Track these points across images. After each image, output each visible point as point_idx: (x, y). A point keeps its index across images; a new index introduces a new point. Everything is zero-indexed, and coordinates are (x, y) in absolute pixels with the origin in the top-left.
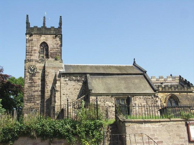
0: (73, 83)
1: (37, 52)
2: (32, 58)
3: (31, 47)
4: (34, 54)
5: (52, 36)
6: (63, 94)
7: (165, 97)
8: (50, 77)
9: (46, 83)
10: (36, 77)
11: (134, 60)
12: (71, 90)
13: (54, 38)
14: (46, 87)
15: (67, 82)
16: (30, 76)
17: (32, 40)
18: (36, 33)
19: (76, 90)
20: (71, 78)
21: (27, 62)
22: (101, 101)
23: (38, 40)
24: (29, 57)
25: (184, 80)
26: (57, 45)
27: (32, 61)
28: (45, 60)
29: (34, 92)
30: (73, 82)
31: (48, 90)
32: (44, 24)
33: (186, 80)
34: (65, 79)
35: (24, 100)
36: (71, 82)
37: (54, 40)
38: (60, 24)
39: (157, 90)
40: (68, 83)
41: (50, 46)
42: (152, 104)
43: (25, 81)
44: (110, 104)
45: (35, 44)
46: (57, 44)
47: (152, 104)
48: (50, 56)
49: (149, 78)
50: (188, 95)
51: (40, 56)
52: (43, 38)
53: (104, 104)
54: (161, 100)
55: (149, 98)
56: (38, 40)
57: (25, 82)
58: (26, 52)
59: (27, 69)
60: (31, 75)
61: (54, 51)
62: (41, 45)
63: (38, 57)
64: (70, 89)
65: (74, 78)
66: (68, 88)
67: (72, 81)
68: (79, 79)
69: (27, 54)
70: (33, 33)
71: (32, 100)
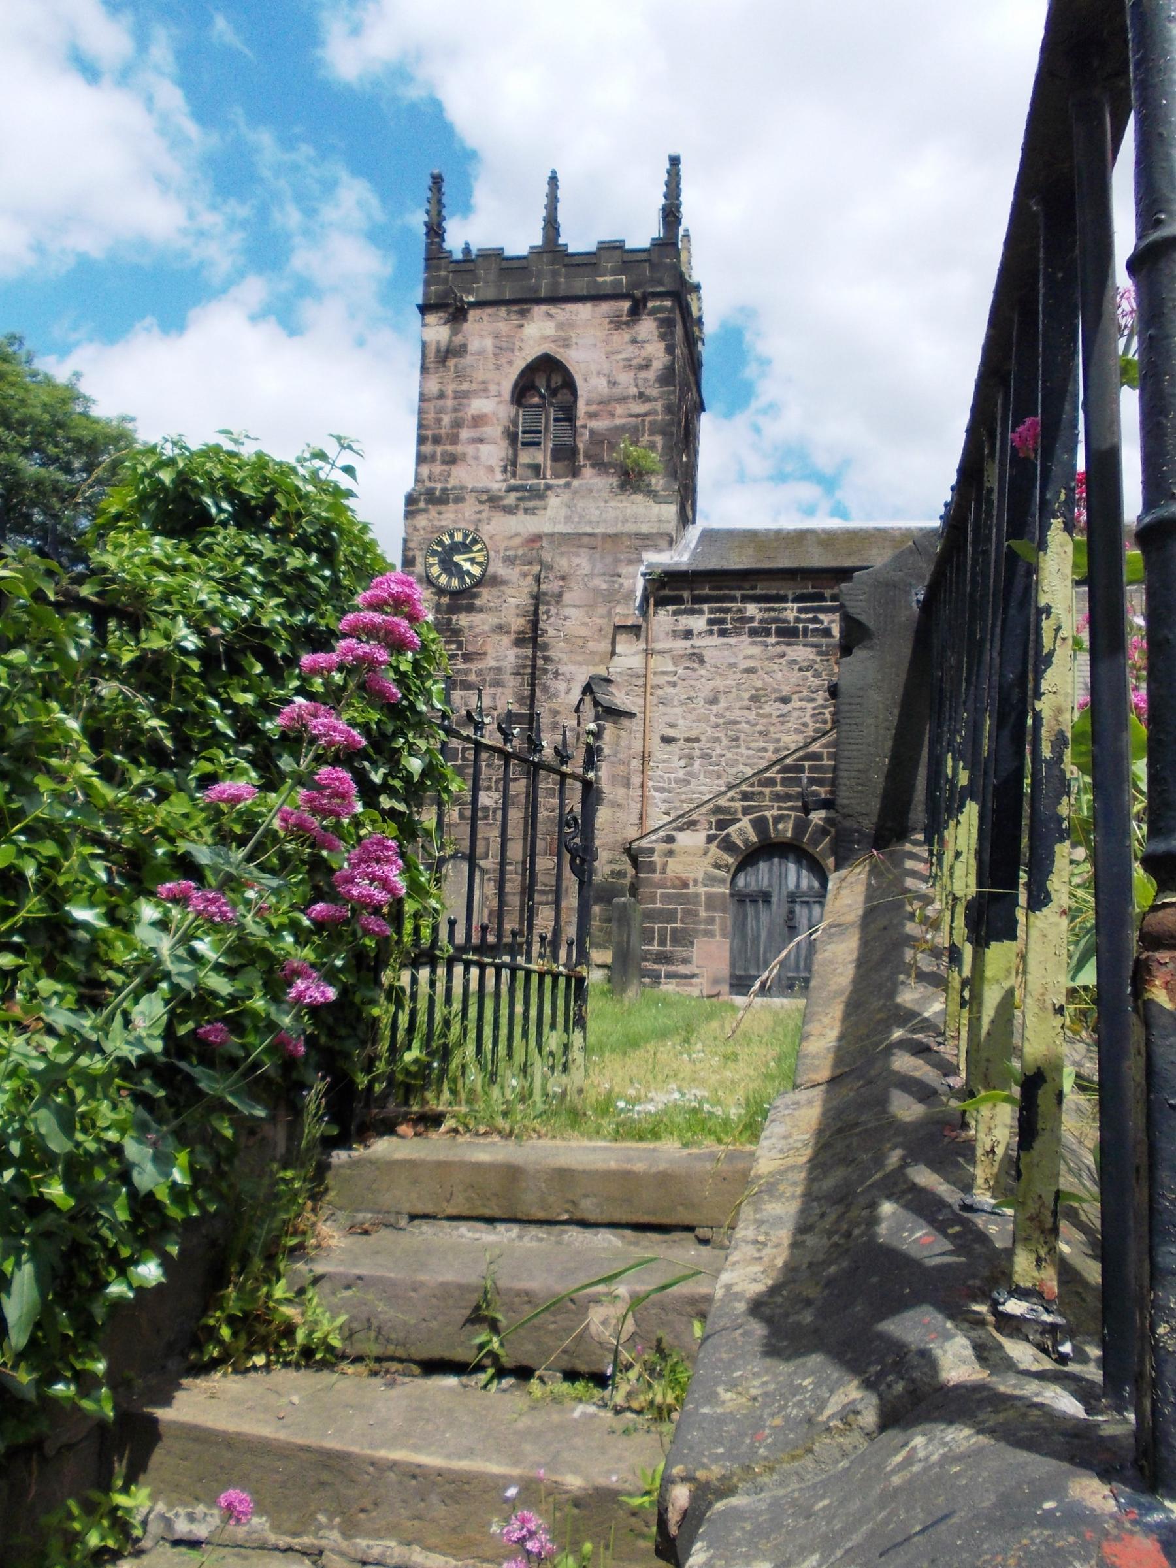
0: (744, 648)
1: (495, 431)
2: (461, 476)
3: (450, 403)
4: (470, 450)
5: (605, 307)
6: (667, 740)
8: (568, 611)
9: (547, 659)
10: (477, 618)
12: (723, 704)
13: (617, 324)
14: (545, 689)
15: (697, 642)
16: (438, 608)
18: (490, 294)
19: (767, 709)
20: (728, 610)
21: (422, 505)
23: (504, 347)
24: (438, 468)
26: (643, 374)
28: (548, 487)
30: (745, 639)
31: (555, 713)
32: (551, 225)
34: (688, 622)
36: (732, 640)
38: (671, 215)
40: (705, 653)
41: (590, 385)
45: (480, 375)
48: (587, 457)
51: (514, 463)
52: (538, 333)
56: (504, 347)
58: (421, 440)
59: (419, 560)
61: (618, 422)
62: (522, 390)
63: (498, 470)
64: (714, 701)
65: (752, 609)
66: (706, 693)
67: (737, 632)
70: (472, 299)
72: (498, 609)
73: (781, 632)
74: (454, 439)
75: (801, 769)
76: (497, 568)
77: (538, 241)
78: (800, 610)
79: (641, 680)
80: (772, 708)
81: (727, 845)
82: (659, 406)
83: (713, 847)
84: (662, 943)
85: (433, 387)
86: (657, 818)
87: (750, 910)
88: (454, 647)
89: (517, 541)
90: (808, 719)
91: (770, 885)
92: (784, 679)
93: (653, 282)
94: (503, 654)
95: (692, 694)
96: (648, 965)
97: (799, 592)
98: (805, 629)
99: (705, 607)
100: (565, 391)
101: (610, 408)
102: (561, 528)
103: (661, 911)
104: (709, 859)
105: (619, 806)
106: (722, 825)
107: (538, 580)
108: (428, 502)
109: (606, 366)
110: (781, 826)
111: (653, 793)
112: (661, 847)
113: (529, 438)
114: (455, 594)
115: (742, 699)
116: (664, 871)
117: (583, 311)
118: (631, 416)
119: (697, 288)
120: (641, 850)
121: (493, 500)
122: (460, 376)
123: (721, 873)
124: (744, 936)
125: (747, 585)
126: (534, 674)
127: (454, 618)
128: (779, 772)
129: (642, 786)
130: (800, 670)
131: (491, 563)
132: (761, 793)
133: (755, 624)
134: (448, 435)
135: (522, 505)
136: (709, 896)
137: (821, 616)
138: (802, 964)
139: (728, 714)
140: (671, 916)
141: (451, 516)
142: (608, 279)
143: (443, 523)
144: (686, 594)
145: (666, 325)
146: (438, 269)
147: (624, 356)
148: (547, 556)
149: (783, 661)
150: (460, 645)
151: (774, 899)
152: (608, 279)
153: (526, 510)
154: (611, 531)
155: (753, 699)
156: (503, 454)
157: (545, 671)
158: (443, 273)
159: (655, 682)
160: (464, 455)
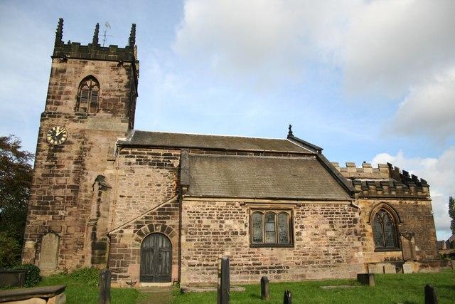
0: (148, 170)
1: (73, 96)
2: (60, 109)
4: (64, 101)
7: (368, 210)
8: (92, 154)
9: (84, 169)
10: (62, 154)
11: (290, 128)
12: (140, 186)
13: (114, 68)
20: (142, 157)
21: (47, 117)
22: (211, 218)
23: (78, 72)
24: (53, 106)
29: (56, 188)
32: (96, 38)
38: (132, 39)
41: (104, 85)
42: (345, 227)
44: (237, 227)
46: (120, 82)
47: (345, 227)
52: (89, 68)
53: (221, 226)
55: (337, 213)
56: (78, 72)
58: (48, 97)
61: (112, 97)
66: (135, 182)
68: (162, 160)
71: (48, 208)
74: (59, 98)
81: (140, 234)
82: (125, 94)
84: (118, 266)
85: (54, 81)
86: (118, 223)
90: (166, 192)
92: (160, 179)
93: (126, 58)
94: (71, 166)
96: (113, 273)
103: (118, 255)
104: (134, 238)
106: (139, 227)
107: (83, 143)
112: (118, 234)
116: (119, 242)
117: (104, 63)
119: (138, 62)
120: (112, 235)
122: (63, 79)
123: (137, 243)
124: (144, 263)
136: (134, 250)
140: (121, 257)
144: (130, 151)
145: (128, 72)
157: (83, 173)
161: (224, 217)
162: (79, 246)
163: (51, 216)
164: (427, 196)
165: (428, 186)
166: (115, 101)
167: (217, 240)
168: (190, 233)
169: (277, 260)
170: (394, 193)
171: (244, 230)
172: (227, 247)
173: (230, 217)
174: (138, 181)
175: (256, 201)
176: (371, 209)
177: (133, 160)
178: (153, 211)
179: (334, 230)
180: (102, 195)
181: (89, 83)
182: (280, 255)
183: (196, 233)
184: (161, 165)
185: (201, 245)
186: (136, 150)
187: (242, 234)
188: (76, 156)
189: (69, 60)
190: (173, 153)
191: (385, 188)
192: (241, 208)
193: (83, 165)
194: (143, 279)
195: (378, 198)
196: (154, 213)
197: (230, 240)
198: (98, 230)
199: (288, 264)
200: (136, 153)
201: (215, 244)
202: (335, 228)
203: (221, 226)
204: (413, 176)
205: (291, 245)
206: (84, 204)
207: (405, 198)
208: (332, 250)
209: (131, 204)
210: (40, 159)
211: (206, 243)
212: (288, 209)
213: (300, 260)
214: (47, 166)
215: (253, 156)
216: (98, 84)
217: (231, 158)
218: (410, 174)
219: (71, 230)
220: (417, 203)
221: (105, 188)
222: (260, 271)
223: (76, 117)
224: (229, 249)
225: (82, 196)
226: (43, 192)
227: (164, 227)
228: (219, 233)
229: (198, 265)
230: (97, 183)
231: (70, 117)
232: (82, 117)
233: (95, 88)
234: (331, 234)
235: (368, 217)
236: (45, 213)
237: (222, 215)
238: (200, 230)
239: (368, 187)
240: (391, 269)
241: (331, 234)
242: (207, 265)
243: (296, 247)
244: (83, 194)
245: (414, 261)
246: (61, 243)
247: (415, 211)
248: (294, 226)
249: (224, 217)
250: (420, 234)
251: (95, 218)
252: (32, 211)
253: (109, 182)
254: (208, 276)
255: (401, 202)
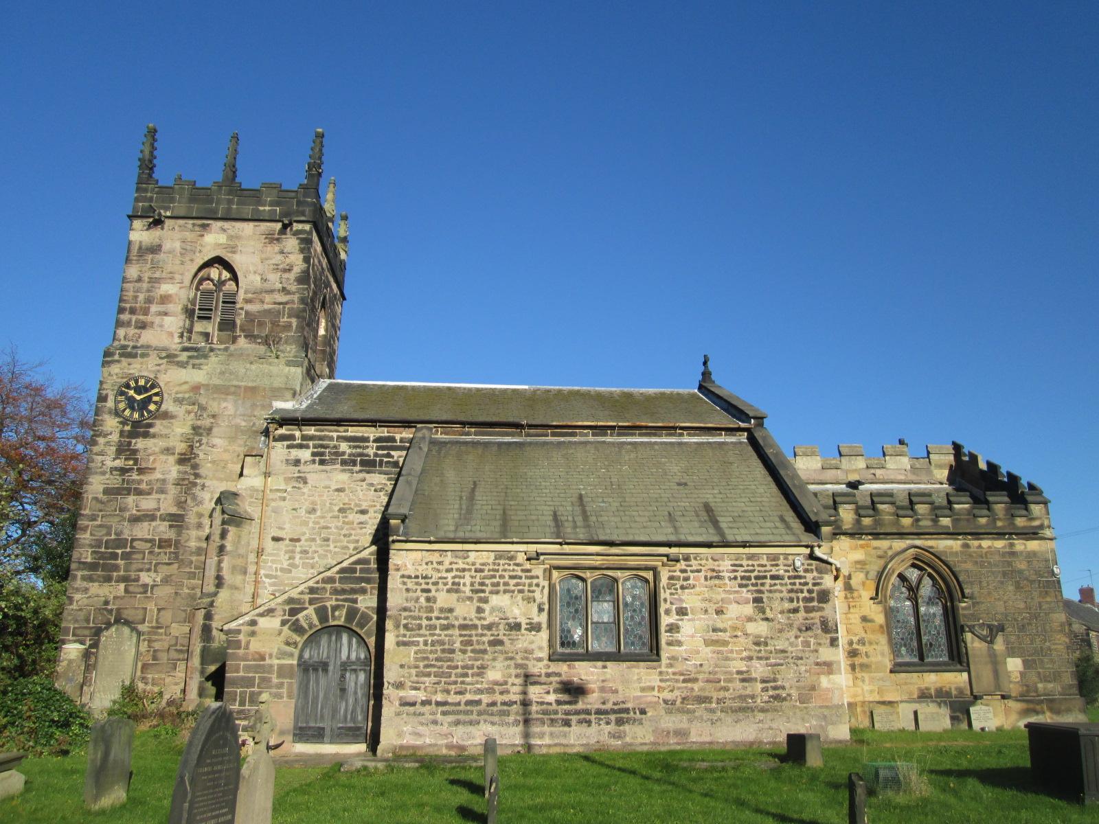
0: (339, 476)
1: (176, 308)
2: (147, 337)
3: (145, 286)
4: (157, 320)
5: (265, 226)
6: (276, 539)
7: (874, 568)
8: (216, 441)
9: (197, 476)
11: (705, 363)
12: (319, 513)
13: (271, 239)
16: (122, 433)
17: (160, 246)
21: (116, 357)
22: (457, 591)
23: (187, 251)
24: (132, 331)
25: (983, 466)
26: (286, 275)
27: (143, 356)
29: (135, 520)
31: (200, 515)
33: (993, 467)
35: (73, 566)
36: (328, 468)
37: (269, 248)
39: (827, 524)
40: (308, 476)
41: (250, 280)
42: (796, 611)
43: (93, 461)
44: (518, 610)
45: (169, 268)
46: (285, 271)
47: (796, 611)
48: (242, 330)
49: (779, 454)
50: (1013, 554)
51: (190, 331)
52: (215, 239)
53: (480, 610)
54: (848, 588)
55: (773, 577)
57: (91, 465)
58: (121, 310)
59: (111, 399)
60: (128, 428)
61: (266, 307)
63: (176, 335)
64: (313, 511)
66: (306, 505)
67: (333, 462)
68: (371, 452)
69: (125, 317)
70: (168, 214)
71: (116, 568)
72: (167, 436)
73: (363, 463)
74: (146, 312)
75: (354, 571)
76: (168, 406)
77: (219, 177)
78: (378, 448)
79: (262, 497)
80: (353, 517)
81: (297, 628)
82: (296, 298)
83: (286, 628)
84: (242, 703)
87: (312, 676)
88: (131, 462)
89: (185, 387)
91: (328, 657)
94: (169, 469)
95: (297, 506)
97: (378, 435)
98: (381, 462)
99: (311, 443)
100: (231, 282)
101: (261, 296)
102: (216, 381)
103: (243, 678)
104: (282, 638)
105: (236, 588)
106: (293, 612)
108: (121, 355)
109: (260, 268)
110: (337, 613)
111: (264, 579)
112: (245, 629)
113: (203, 313)
114: (136, 424)
115: (333, 511)
116: (247, 647)
117: (248, 228)
118: (275, 303)
121: (170, 357)
122: (155, 267)
125: (342, 429)
126: (188, 485)
127: (134, 441)
128: (338, 572)
129: (255, 574)
130: (375, 491)
131: (165, 402)
132: (324, 588)
133: (346, 457)
134: (141, 308)
135: (193, 361)
136: (281, 667)
137: (393, 453)
138: (349, 717)
139: (322, 521)
140: (249, 682)
141: (138, 366)
142: (267, 208)
143: (131, 372)
144: (297, 434)
146: (146, 190)
147: (274, 261)
148: (203, 401)
149: (364, 483)
150: (136, 461)
151: (331, 668)
152: (267, 208)
153: (194, 366)
154: (250, 384)
155: (341, 510)
156: (181, 324)
157: (195, 484)
158: (149, 195)
159: (271, 497)
160: (152, 323)
161: (488, 589)
162: (181, 656)
163: (122, 586)
164: (1041, 527)
165: (1045, 503)
166: (273, 315)
167: (470, 643)
168: (406, 626)
169: (616, 691)
170: (945, 521)
171: (536, 620)
172: (494, 659)
173: (502, 588)
174: (314, 503)
175: (567, 549)
176: (881, 562)
177: (305, 455)
178: (328, 574)
179: (767, 619)
180: (230, 536)
181: (214, 273)
182: (626, 682)
183: (420, 627)
184: (369, 465)
185: (431, 656)
186: (311, 431)
187: (529, 630)
188: (181, 447)
189: (168, 223)
190: (398, 437)
191: (922, 509)
192: (528, 566)
193: (195, 467)
194: (303, 733)
195: (901, 535)
196: (330, 580)
197: (501, 643)
198: (216, 617)
199: (646, 705)
200: (311, 438)
201: (464, 652)
202: (769, 614)
203: (480, 610)
204: (1010, 475)
205: (653, 653)
206: (194, 558)
207: (977, 535)
208: (759, 669)
209: (298, 556)
210: (102, 453)
211: (443, 651)
212: (647, 569)
213: (677, 693)
214: (116, 469)
215: (591, 438)
216: (235, 278)
217: (537, 443)
218: (1004, 470)
219: (167, 617)
220: (1012, 545)
221: (234, 519)
222: (574, 718)
223: (184, 356)
224: (499, 664)
225: (193, 539)
226: (104, 531)
227: (352, 613)
228: (475, 627)
229: (424, 703)
230: (219, 508)
231: (168, 356)
232: (196, 355)
233: (230, 286)
234: (759, 628)
235: (873, 586)
236: (108, 579)
237: (482, 584)
238: (429, 619)
239: (874, 509)
240: (937, 719)
241: (759, 628)
242: (445, 703)
243: (664, 661)
244: (194, 533)
245: (1003, 697)
246: (144, 647)
247: (1008, 571)
248: (662, 610)
249: (488, 589)
250: (1022, 628)
251: (212, 589)
252: (79, 574)
253: (248, 507)
254: (445, 729)
255: (966, 546)
